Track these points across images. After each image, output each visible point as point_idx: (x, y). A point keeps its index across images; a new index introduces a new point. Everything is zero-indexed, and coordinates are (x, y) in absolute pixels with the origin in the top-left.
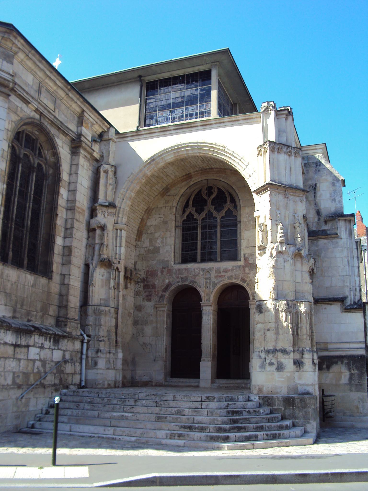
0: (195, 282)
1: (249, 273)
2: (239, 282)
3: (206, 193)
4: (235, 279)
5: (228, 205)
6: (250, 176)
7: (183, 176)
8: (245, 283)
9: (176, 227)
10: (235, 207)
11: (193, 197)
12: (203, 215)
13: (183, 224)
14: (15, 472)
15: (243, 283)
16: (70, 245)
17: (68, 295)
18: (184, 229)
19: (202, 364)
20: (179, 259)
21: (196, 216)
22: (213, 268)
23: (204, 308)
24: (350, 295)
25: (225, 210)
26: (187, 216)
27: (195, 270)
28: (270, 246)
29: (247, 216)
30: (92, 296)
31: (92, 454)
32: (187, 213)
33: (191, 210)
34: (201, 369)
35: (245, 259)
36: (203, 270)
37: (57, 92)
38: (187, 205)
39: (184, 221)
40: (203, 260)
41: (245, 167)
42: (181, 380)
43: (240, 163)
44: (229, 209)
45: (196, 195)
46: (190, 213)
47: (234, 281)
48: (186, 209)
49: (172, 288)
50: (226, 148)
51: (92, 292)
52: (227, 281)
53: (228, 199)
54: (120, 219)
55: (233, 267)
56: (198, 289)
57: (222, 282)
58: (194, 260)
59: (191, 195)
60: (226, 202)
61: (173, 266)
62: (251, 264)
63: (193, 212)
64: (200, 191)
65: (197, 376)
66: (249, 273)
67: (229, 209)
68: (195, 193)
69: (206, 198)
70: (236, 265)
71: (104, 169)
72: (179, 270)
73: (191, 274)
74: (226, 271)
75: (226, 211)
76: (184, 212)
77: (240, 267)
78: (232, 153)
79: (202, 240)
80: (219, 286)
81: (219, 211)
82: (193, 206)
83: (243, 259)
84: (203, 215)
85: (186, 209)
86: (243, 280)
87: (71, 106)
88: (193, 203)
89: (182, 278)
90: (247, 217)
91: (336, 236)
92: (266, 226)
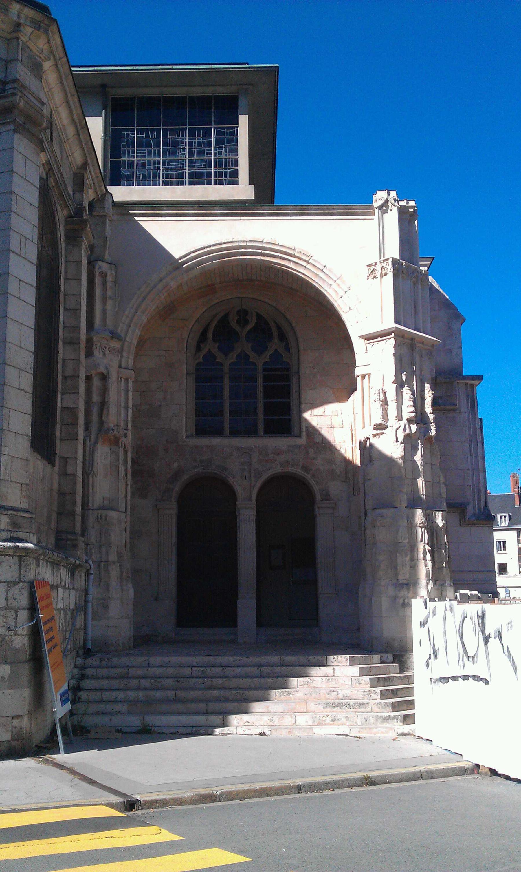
0: (226, 469)
1: (314, 458)
2: (298, 471)
3: (237, 320)
4: (293, 466)
5: (275, 345)
6: (350, 309)
7: (201, 288)
8: (308, 473)
9: (187, 374)
10: (287, 348)
11: (213, 325)
12: (233, 357)
13: (197, 370)
14: (111, 837)
15: (305, 474)
16: (74, 406)
17: (75, 493)
18: (198, 379)
19: (240, 603)
20: (192, 430)
21: (220, 358)
22: (256, 447)
23: (242, 512)
24: (474, 500)
25: (270, 352)
26: (205, 356)
27: (225, 449)
28: (392, 422)
29: (311, 365)
30: (93, 492)
31: (55, 767)
32: (204, 352)
33: (211, 346)
34: (239, 613)
35: (307, 435)
36: (238, 449)
37: (65, 130)
38: (203, 337)
39: (198, 364)
40: (234, 433)
41: (341, 293)
42: (201, 631)
43: (334, 286)
44: (276, 350)
45: (218, 322)
46: (209, 351)
47: (290, 469)
48: (202, 345)
49: (185, 477)
50: (312, 258)
51: (93, 486)
52: (279, 469)
53: (275, 333)
54: (123, 360)
55: (289, 446)
56: (231, 480)
57: (270, 471)
58: (219, 432)
59: (211, 321)
60: (271, 338)
61: (186, 440)
62: (318, 443)
63: (215, 350)
64: (226, 316)
65: (233, 623)
66: (314, 458)
67: (276, 350)
68: (218, 318)
69: (237, 328)
70: (294, 444)
71: (100, 270)
72: (197, 447)
73: (217, 455)
74: (278, 452)
75: (271, 353)
76: (198, 349)
77: (299, 447)
78: (321, 267)
79: (230, 399)
80: (264, 477)
81: (260, 353)
82: (214, 340)
83: (304, 434)
84: (233, 357)
85: (202, 345)
86: (306, 469)
87: (73, 153)
88: (213, 337)
89: (201, 461)
90: (310, 367)
91: (453, 407)
92: (385, 393)
